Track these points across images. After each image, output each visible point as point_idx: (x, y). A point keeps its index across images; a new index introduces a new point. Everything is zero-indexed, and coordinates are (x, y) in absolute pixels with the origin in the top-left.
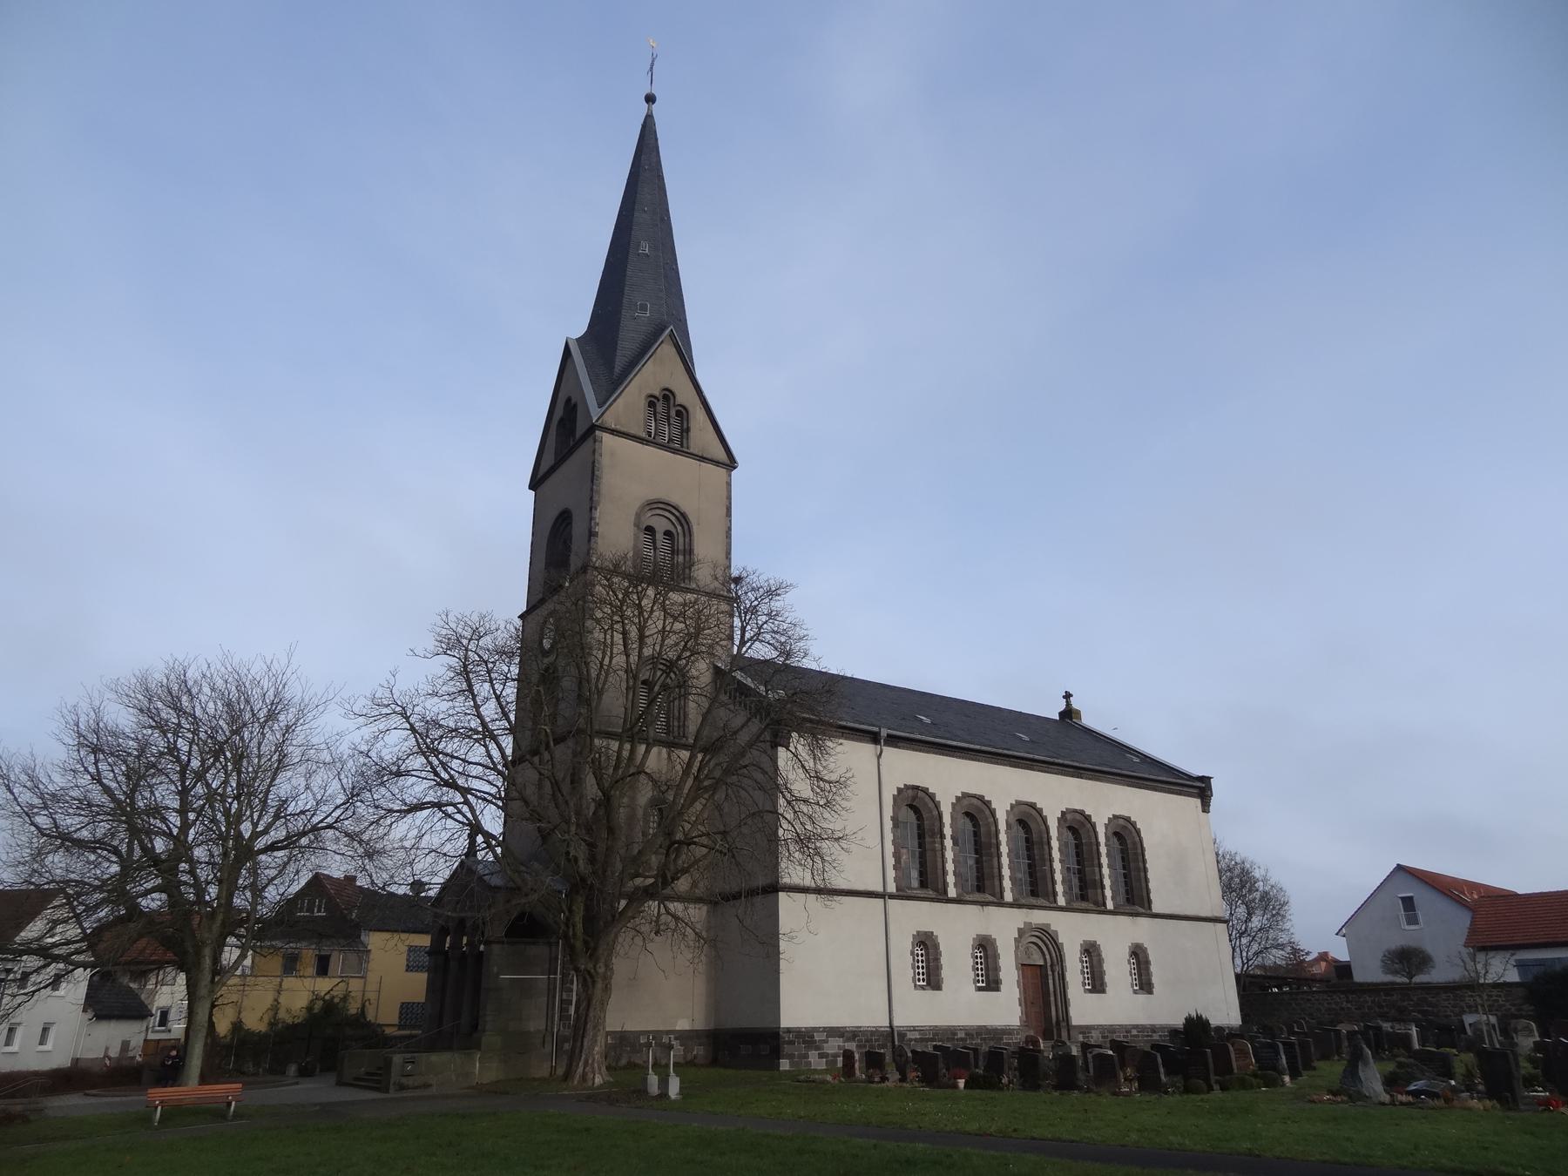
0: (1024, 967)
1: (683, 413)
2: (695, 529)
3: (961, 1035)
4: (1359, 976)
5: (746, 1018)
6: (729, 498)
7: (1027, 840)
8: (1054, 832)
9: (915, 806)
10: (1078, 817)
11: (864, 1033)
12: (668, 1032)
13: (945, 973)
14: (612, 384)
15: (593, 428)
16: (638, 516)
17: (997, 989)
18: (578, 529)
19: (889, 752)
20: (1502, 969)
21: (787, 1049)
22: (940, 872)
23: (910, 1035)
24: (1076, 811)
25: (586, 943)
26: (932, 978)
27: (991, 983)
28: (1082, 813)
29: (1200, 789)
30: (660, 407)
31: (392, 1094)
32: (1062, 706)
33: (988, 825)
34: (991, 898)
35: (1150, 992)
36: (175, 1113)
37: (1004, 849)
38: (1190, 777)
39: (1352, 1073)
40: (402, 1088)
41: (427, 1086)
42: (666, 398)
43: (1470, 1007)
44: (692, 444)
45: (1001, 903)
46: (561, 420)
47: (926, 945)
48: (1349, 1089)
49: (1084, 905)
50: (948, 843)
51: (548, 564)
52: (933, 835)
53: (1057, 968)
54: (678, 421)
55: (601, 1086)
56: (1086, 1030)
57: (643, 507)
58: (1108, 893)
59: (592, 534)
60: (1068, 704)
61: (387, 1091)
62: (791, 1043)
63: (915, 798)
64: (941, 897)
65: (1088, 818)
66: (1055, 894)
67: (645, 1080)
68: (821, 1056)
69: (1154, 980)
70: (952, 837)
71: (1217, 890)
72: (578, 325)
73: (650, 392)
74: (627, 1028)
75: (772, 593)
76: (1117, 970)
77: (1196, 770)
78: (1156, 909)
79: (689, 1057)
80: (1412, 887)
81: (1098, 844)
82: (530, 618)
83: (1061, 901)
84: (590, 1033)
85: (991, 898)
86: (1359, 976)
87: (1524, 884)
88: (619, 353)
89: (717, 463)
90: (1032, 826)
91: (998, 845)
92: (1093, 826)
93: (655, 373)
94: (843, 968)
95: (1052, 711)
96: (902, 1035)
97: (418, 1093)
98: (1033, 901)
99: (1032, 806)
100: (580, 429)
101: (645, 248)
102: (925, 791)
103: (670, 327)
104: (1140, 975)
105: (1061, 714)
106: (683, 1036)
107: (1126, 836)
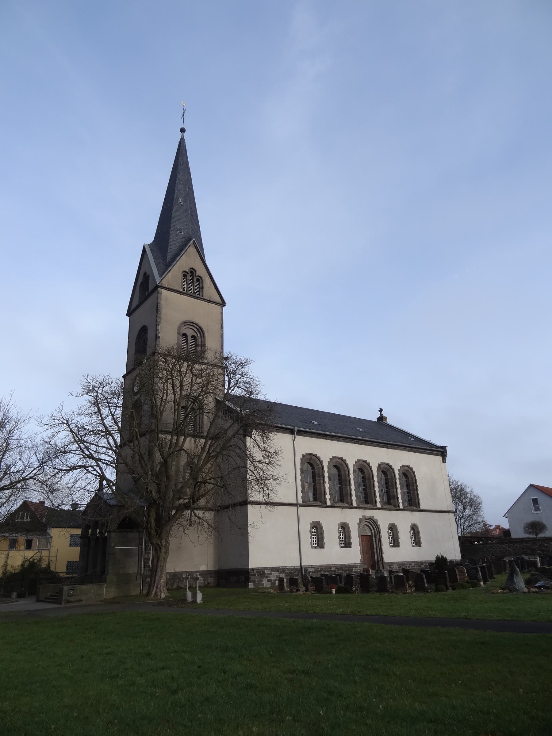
0: (362, 536)
1: (200, 280)
2: (206, 335)
3: (333, 569)
4: (514, 536)
5: (232, 564)
6: (222, 320)
7: (363, 478)
8: (375, 474)
9: (311, 462)
12: (196, 572)
13: (325, 540)
14: (166, 266)
15: (157, 287)
16: (179, 328)
17: (350, 547)
18: (150, 335)
19: (299, 438)
21: (252, 578)
22: (323, 493)
23: (310, 570)
24: (385, 464)
25: (156, 531)
26: (320, 543)
28: (388, 464)
29: (442, 452)
30: (189, 277)
31: (63, 605)
33: (345, 471)
34: (346, 505)
35: (420, 546)
39: (511, 579)
40: (68, 602)
41: (80, 601)
42: (191, 272)
45: (351, 507)
46: (142, 283)
47: (317, 527)
49: (389, 507)
50: (327, 480)
52: (319, 477)
53: (377, 536)
54: (198, 284)
55: (164, 598)
56: (391, 564)
57: (181, 325)
58: (400, 501)
59: (157, 337)
60: (381, 414)
62: (255, 575)
63: (311, 459)
66: (376, 502)
68: (268, 581)
69: (422, 540)
70: (328, 477)
72: (150, 238)
74: (177, 570)
75: (243, 364)
76: (405, 536)
77: (440, 444)
78: (422, 507)
79: (206, 583)
81: (395, 479)
83: (379, 505)
84: (159, 574)
85: (346, 505)
88: (169, 251)
89: (216, 303)
91: (350, 480)
92: (393, 470)
94: (278, 539)
95: (374, 417)
96: (306, 570)
97: (76, 604)
99: (365, 462)
100: (151, 288)
102: (315, 456)
103: (193, 239)
104: (415, 538)
105: (378, 419)
107: (408, 474)
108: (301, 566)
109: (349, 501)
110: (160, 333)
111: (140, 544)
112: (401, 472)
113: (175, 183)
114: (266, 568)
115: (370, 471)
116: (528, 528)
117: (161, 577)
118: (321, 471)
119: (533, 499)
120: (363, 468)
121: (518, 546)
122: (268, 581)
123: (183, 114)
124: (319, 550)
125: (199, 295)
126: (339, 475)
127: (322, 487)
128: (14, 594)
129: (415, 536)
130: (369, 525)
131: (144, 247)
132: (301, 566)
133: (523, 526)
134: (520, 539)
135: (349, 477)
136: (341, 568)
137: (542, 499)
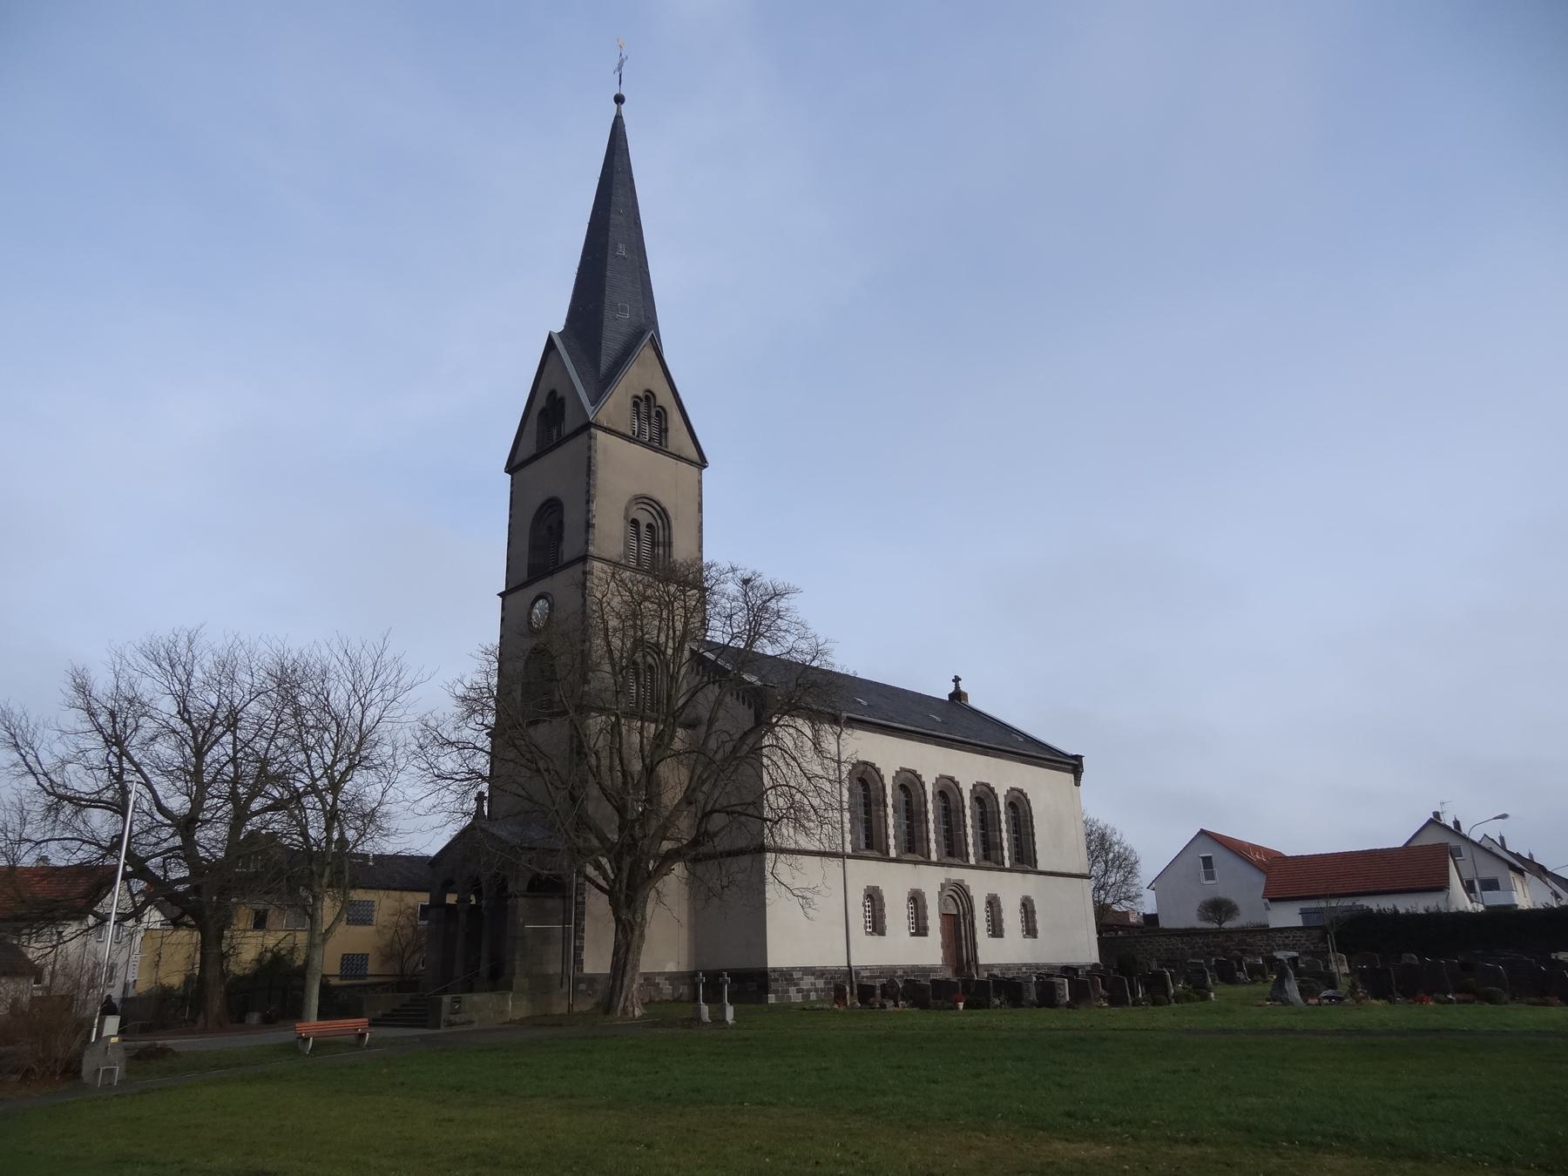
0: (945, 916)
1: (662, 414)
2: (674, 523)
4: (1163, 924)
5: (733, 959)
7: (945, 808)
8: (967, 802)
9: (865, 778)
13: (887, 921)
14: (602, 386)
15: (588, 426)
16: (627, 510)
18: (571, 518)
20: (1287, 916)
21: (773, 985)
25: (627, 896)
26: (877, 926)
27: (920, 930)
28: (987, 785)
29: (1073, 765)
30: (643, 408)
32: (952, 688)
36: (293, 1049)
37: (931, 816)
38: (1066, 756)
39: (1280, 984)
40: (450, 1024)
41: (471, 1022)
45: (929, 863)
46: (543, 413)
47: (874, 897)
48: (1278, 994)
49: (988, 864)
50: (890, 810)
51: (533, 548)
52: (878, 805)
54: (659, 421)
55: (641, 1018)
56: (989, 967)
57: (630, 502)
59: (589, 526)
60: (957, 687)
62: (776, 980)
64: (885, 857)
65: (992, 790)
66: (967, 854)
67: (699, 1009)
68: (799, 991)
75: (777, 595)
78: (1040, 868)
80: (1213, 849)
82: (508, 598)
83: (972, 861)
86: (1163, 924)
87: (1289, 851)
89: (690, 462)
90: (951, 797)
91: (926, 812)
94: (822, 917)
95: (943, 691)
96: (857, 973)
97: (465, 1028)
98: (951, 860)
99: (951, 779)
100: (568, 426)
101: (622, 250)
102: (872, 766)
106: (673, 978)
107: (1019, 804)
111: (566, 921)
117: (633, 980)
120: (909, 784)
122: (799, 991)
123: (620, 68)
126: (907, 803)
128: (254, 1018)
133: (1197, 905)
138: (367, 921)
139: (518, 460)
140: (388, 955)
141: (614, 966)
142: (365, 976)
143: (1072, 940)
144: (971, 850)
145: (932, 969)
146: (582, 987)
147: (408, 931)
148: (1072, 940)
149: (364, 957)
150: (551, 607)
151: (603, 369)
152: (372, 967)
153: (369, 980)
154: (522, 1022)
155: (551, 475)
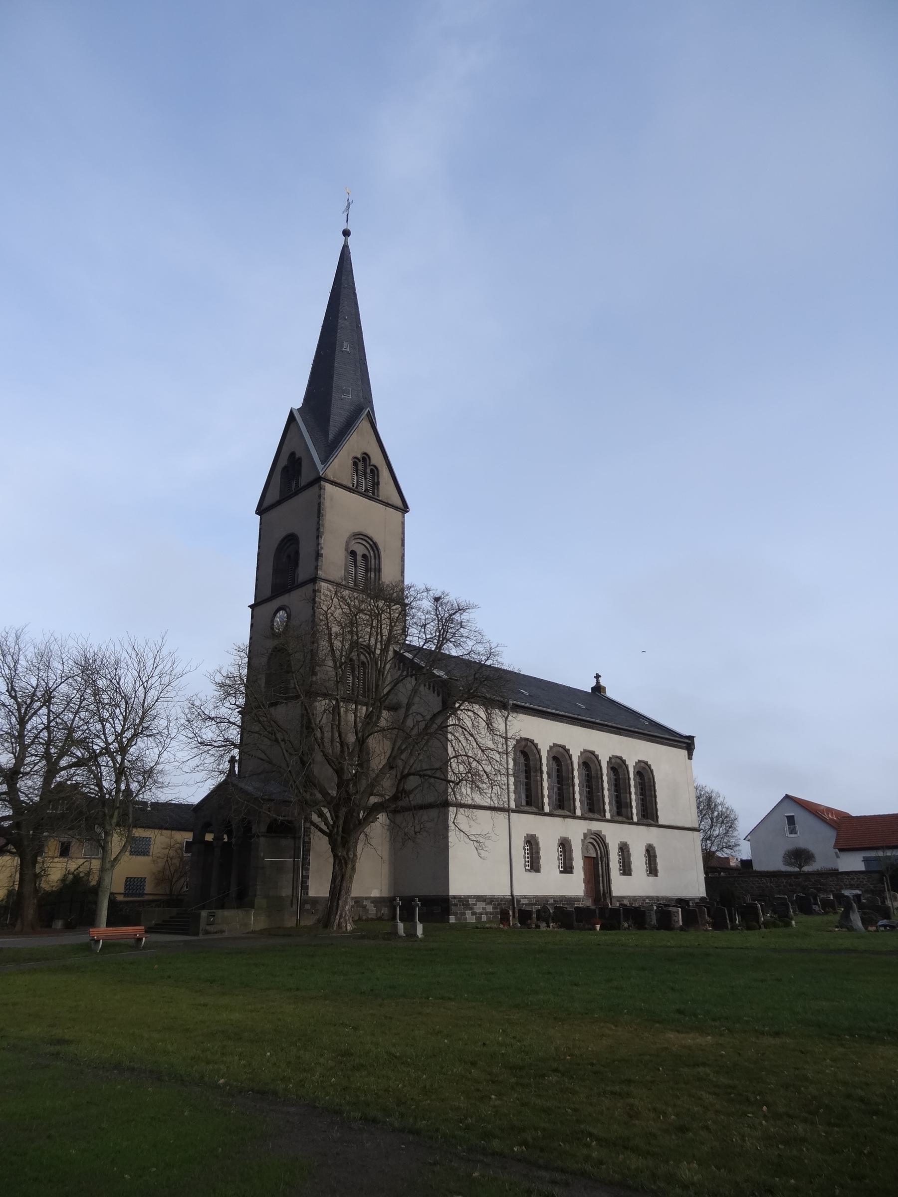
0: (586, 858)
1: (375, 471)
3: (551, 901)
4: (756, 867)
6: (403, 533)
7: (588, 775)
9: (526, 751)
10: (619, 761)
11: (497, 899)
12: (367, 898)
13: (542, 861)
14: (330, 449)
15: (318, 480)
16: (347, 543)
17: (571, 872)
18: (305, 549)
20: (853, 863)
22: (540, 795)
23: (523, 901)
24: (617, 757)
25: (342, 837)
26: (534, 865)
27: (567, 868)
29: (687, 744)
31: (201, 937)
32: (594, 683)
33: (567, 765)
34: (568, 813)
35: (656, 876)
37: (576, 781)
38: (681, 736)
40: (207, 932)
41: (222, 932)
42: (364, 459)
43: (846, 885)
44: (380, 494)
45: (574, 817)
46: (285, 469)
47: (532, 843)
49: (620, 819)
50: (545, 776)
51: (276, 571)
52: (536, 771)
54: (373, 477)
57: (350, 538)
58: (634, 811)
59: (318, 555)
60: (598, 682)
61: (198, 935)
62: (456, 905)
63: (526, 746)
64: (540, 812)
66: (604, 811)
68: (473, 914)
69: (659, 868)
70: (547, 773)
71: (695, 810)
72: (298, 403)
73: (355, 455)
75: (460, 610)
76: (638, 861)
77: (685, 732)
79: (379, 915)
80: (795, 810)
81: (629, 779)
83: (608, 816)
84: (343, 898)
85: (568, 813)
89: (396, 508)
90: (592, 766)
91: (573, 778)
92: (627, 767)
93: (356, 443)
94: (492, 857)
95: (587, 686)
96: (518, 901)
97: (216, 936)
98: (591, 815)
99: (593, 753)
101: (347, 347)
102: (532, 741)
103: (362, 409)
104: (650, 864)
107: (645, 773)
108: (512, 895)
109: (572, 808)
110: (322, 548)
112: (581, 761)
113: (336, 317)
114: (469, 897)
115: (569, 762)
116: (790, 858)
117: (346, 902)
118: (538, 763)
119: (788, 817)
121: (785, 881)
122: (473, 914)
123: (347, 209)
124: (534, 874)
125: (373, 494)
126: (558, 771)
127: (540, 787)
128: (59, 924)
129: (649, 860)
130: (595, 843)
131: (291, 412)
132: (512, 895)
134: (768, 872)
135: (573, 773)
136: (561, 901)
137: (802, 817)
138: (145, 853)
139: (265, 505)
140: (162, 878)
141: (332, 891)
142: (143, 894)
143: (685, 880)
144: (607, 807)
145: (576, 899)
146: (308, 907)
147: (176, 861)
148: (685, 880)
149: (143, 880)
150: (289, 616)
151: (331, 436)
152: (149, 888)
153: (146, 898)
154: (261, 932)
155: (290, 518)
